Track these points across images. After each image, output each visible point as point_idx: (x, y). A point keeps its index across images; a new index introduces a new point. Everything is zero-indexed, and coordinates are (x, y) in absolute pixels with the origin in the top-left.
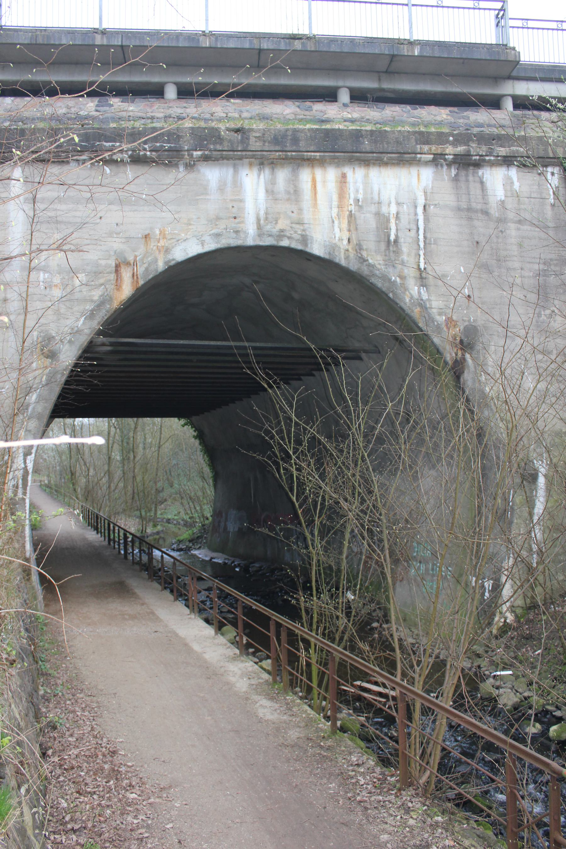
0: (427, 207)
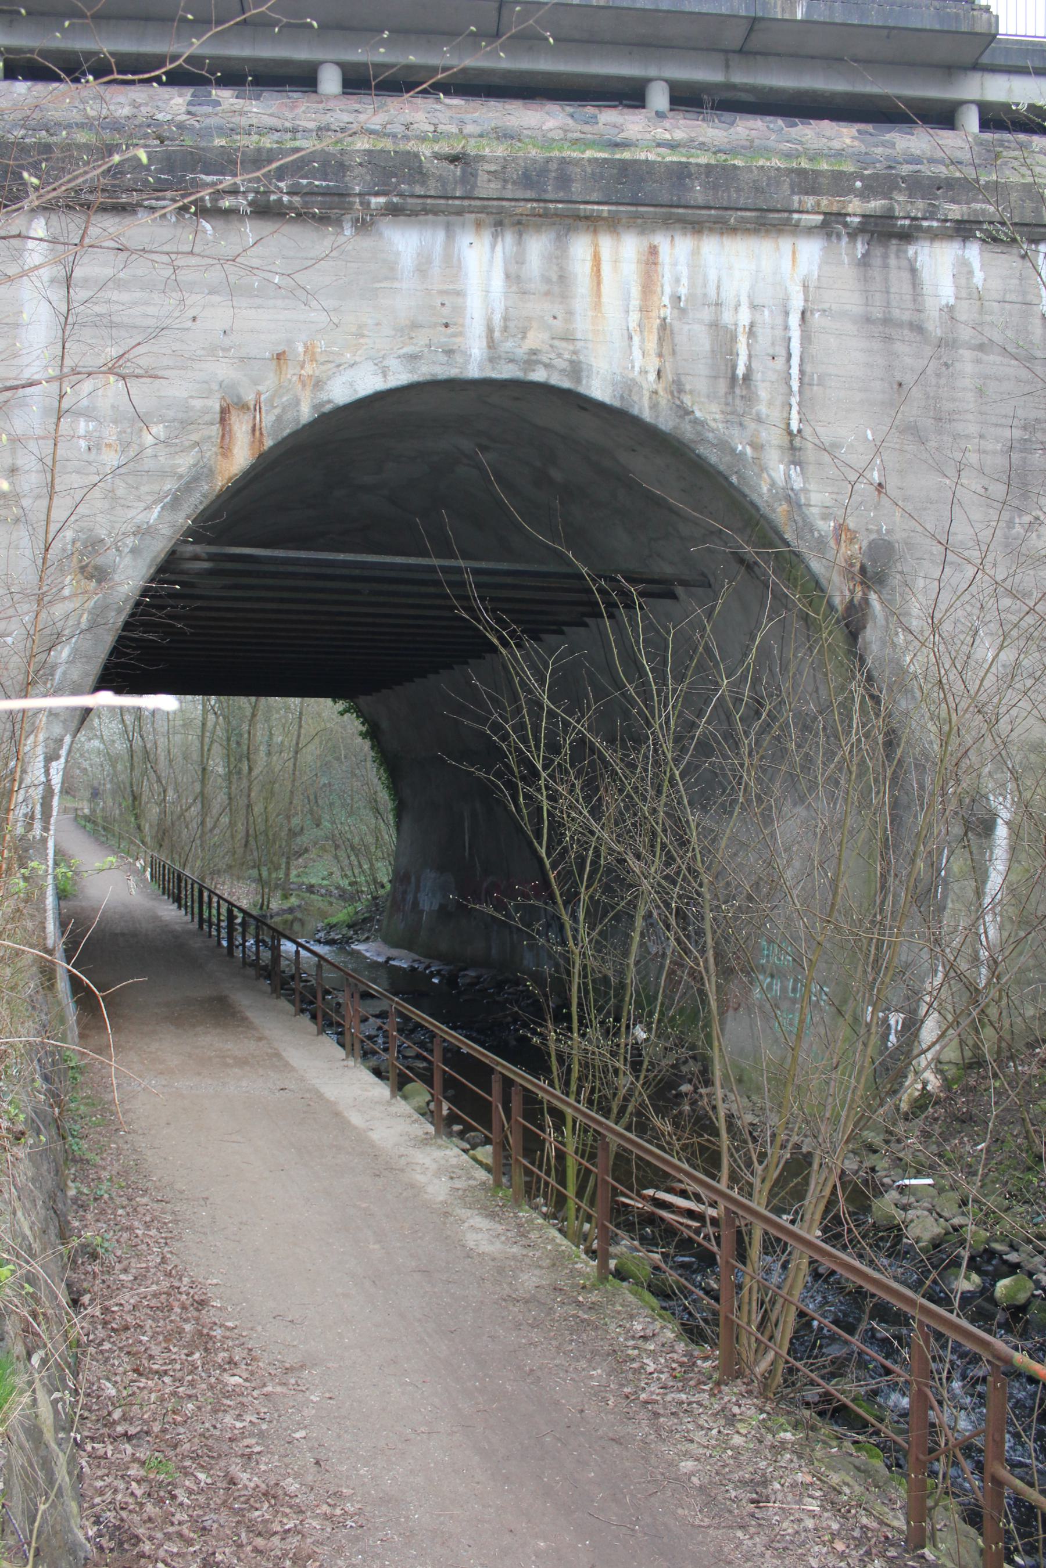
0: (808, 314)
